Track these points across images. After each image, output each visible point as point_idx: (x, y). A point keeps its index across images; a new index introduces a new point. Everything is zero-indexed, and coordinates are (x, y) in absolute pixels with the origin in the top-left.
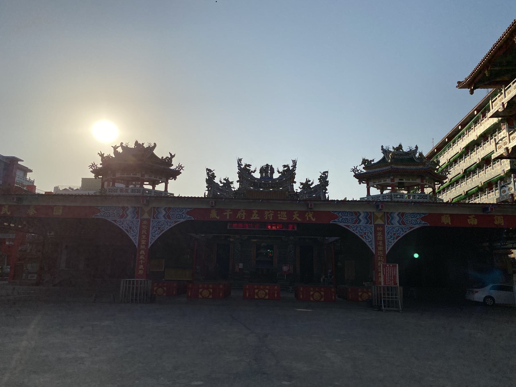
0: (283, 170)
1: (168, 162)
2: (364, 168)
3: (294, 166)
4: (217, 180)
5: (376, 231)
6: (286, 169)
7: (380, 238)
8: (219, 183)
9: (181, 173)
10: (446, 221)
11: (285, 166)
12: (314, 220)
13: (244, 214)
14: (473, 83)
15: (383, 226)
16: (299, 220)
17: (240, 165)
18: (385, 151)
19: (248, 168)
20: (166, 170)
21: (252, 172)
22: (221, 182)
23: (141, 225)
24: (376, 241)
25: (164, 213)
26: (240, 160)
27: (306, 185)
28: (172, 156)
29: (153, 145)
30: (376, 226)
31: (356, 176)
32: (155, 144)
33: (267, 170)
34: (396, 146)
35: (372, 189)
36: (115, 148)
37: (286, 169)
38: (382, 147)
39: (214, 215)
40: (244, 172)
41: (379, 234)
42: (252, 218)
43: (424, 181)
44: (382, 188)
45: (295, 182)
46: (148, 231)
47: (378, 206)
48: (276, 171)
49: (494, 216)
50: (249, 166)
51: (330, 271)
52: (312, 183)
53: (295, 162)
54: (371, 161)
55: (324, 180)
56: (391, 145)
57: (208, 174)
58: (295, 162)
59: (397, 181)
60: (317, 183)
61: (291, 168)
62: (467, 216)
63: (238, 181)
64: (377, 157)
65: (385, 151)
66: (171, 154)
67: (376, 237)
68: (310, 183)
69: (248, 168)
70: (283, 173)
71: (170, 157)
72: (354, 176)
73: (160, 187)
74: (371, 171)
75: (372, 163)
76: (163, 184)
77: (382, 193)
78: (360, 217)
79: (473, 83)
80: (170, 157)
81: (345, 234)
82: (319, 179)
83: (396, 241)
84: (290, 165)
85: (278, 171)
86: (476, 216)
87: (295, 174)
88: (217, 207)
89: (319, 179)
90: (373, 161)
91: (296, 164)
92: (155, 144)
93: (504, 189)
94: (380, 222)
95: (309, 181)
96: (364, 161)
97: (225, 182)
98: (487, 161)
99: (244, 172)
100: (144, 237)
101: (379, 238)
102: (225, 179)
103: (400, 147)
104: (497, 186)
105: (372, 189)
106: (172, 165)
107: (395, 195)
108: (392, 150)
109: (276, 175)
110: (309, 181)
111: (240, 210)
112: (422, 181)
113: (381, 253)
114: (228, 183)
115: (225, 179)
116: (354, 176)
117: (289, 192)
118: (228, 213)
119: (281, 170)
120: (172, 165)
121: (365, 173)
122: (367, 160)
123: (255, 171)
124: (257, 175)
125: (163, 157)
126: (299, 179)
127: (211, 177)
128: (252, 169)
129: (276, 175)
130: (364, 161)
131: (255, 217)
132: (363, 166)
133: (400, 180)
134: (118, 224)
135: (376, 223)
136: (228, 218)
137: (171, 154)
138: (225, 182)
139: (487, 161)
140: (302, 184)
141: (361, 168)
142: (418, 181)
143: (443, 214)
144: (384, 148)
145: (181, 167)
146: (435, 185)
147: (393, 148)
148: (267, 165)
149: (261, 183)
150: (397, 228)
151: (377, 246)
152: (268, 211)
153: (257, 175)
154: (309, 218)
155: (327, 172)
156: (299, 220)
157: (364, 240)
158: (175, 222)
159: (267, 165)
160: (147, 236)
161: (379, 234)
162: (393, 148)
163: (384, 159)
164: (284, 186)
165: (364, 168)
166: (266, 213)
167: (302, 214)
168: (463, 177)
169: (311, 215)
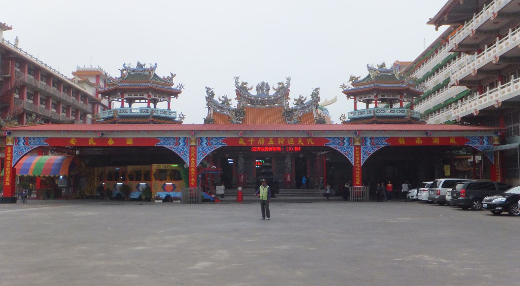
0: (278, 87)
1: (169, 81)
2: (351, 84)
3: (288, 84)
4: (216, 98)
5: (355, 151)
6: (281, 86)
7: (357, 155)
8: (218, 101)
9: (181, 92)
10: (402, 142)
11: (280, 84)
12: (313, 144)
13: (263, 141)
14: (437, 21)
15: (359, 146)
16: (303, 144)
17: (237, 83)
18: (370, 69)
19: (245, 85)
20: (166, 90)
21: (249, 89)
22: (220, 100)
23: (190, 150)
24: (355, 157)
25: (206, 141)
26: (237, 78)
27: (300, 102)
28: (173, 76)
29: (154, 65)
30: (355, 146)
31: (345, 92)
32: (156, 64)
33: (263, 87)
34: (380, 64)
35: (359, 103)
36: (122, 71)
37: (281, 86)
38: (368, 65)
39: (241, 142)
40: (242, 91)
41: (357, 152)
42: (269, 144)
43: (403, 97)
44: (368, 102)
45: (289, 99)
46: (195, 155)
47: (356, 134)
48: (271, 88)
49: (433, 137)
50: (246, 83)
51: (322, 178)
52: (305, 99)
53: (289, 79)
54: (358, 78)
55: (315, 96)
56: (376, 64)
57: (207, 92)
58: (289, 79)
59: (380, 97)
60: (309, 98)
61: (285, 85)
62: (415, 138)
63: (236, 99)
64: (363, 74)
65: (370, 69)
66: (172, 74)
67: (355, 154)
68: (303, 99)
69: (245, 85)
70: (278, 90)
71: (171, 76)
72: (343, 92)
73: (162, 105)
74: (358, 87)
75: (359, 79)
76: (166, 103)
77: (367, 107)
78: (345, 141)
79: (437, 21)
80: (171, 76)
81: (334, 153)
82: (311, 95)
83: (368, 156)
84: (285, 83)
85: (274, 88)
86: (422, 138)
87: (289, 91)
88: (244, 136)
89: (311, 95)
90: (360, 78)
91: (290, 82)
92: (156, 64)
93: (457, 110)
94: (357, 144)
95: (303, 97)
96: (352, 79)
97: (224, 99)
98: (445, 84)
99: (242, 91)
100: (193, 158)
101: (357, 155)
102: (223, 97)
103: (383, 65)
104: (451, 106)
105: (359, 103)
106: (173, 84)
107: (377, 110)
108: (377, 68)
109: (272, 92)
110: (303, 97)
111: (260, 138)
112: (401, 97)
113: (358, 165)
114: (226, 101)
115: (223, 97)
116: (343, 92)
117: (285, 110)
118: (252, 141)
119: (276, 87)
120: (173, 84)
121: (353, 89)
122: (354, 77)
123: (252, 88)
124: (254, 92)
125: (164, 77)
126: (293, 96)
127: (210, 96)
128: (249, 86)
129: (272, 92)
130: (352, 79)
131: (271, 143)
132: (351, 82)
133: (382, 96)
134: (173, 150)
135: (355, 144)
136: (252, 144)
137: (172, 74)
138: (224, 99)
139: (445, 84)
140: (296, 100)
141: (349, 86)
142: (398, 97)
143: (400, 137)
144: (370, 65)
145: (181, 86)
146: (413, 99)
147: (378, 65)
148: (263, 82)
149: (257, 101)
150: (369, 148)
151: (355, 160)
152: (281, 138)
153: (254, 92)
154: (310, 142)
155: (319, 88)
156: (303, 144)
157: (347, 157)
158: (215, 148)
159: (263, 82)
160: (195, 158)
161: (357, 152)
162: (378, 65)
163: (369, 75)
164: (279, 102)
165: (351, 84)
166: (279, 140)
167: (304, 140)
168: (434, 93)
169: (311, 141)
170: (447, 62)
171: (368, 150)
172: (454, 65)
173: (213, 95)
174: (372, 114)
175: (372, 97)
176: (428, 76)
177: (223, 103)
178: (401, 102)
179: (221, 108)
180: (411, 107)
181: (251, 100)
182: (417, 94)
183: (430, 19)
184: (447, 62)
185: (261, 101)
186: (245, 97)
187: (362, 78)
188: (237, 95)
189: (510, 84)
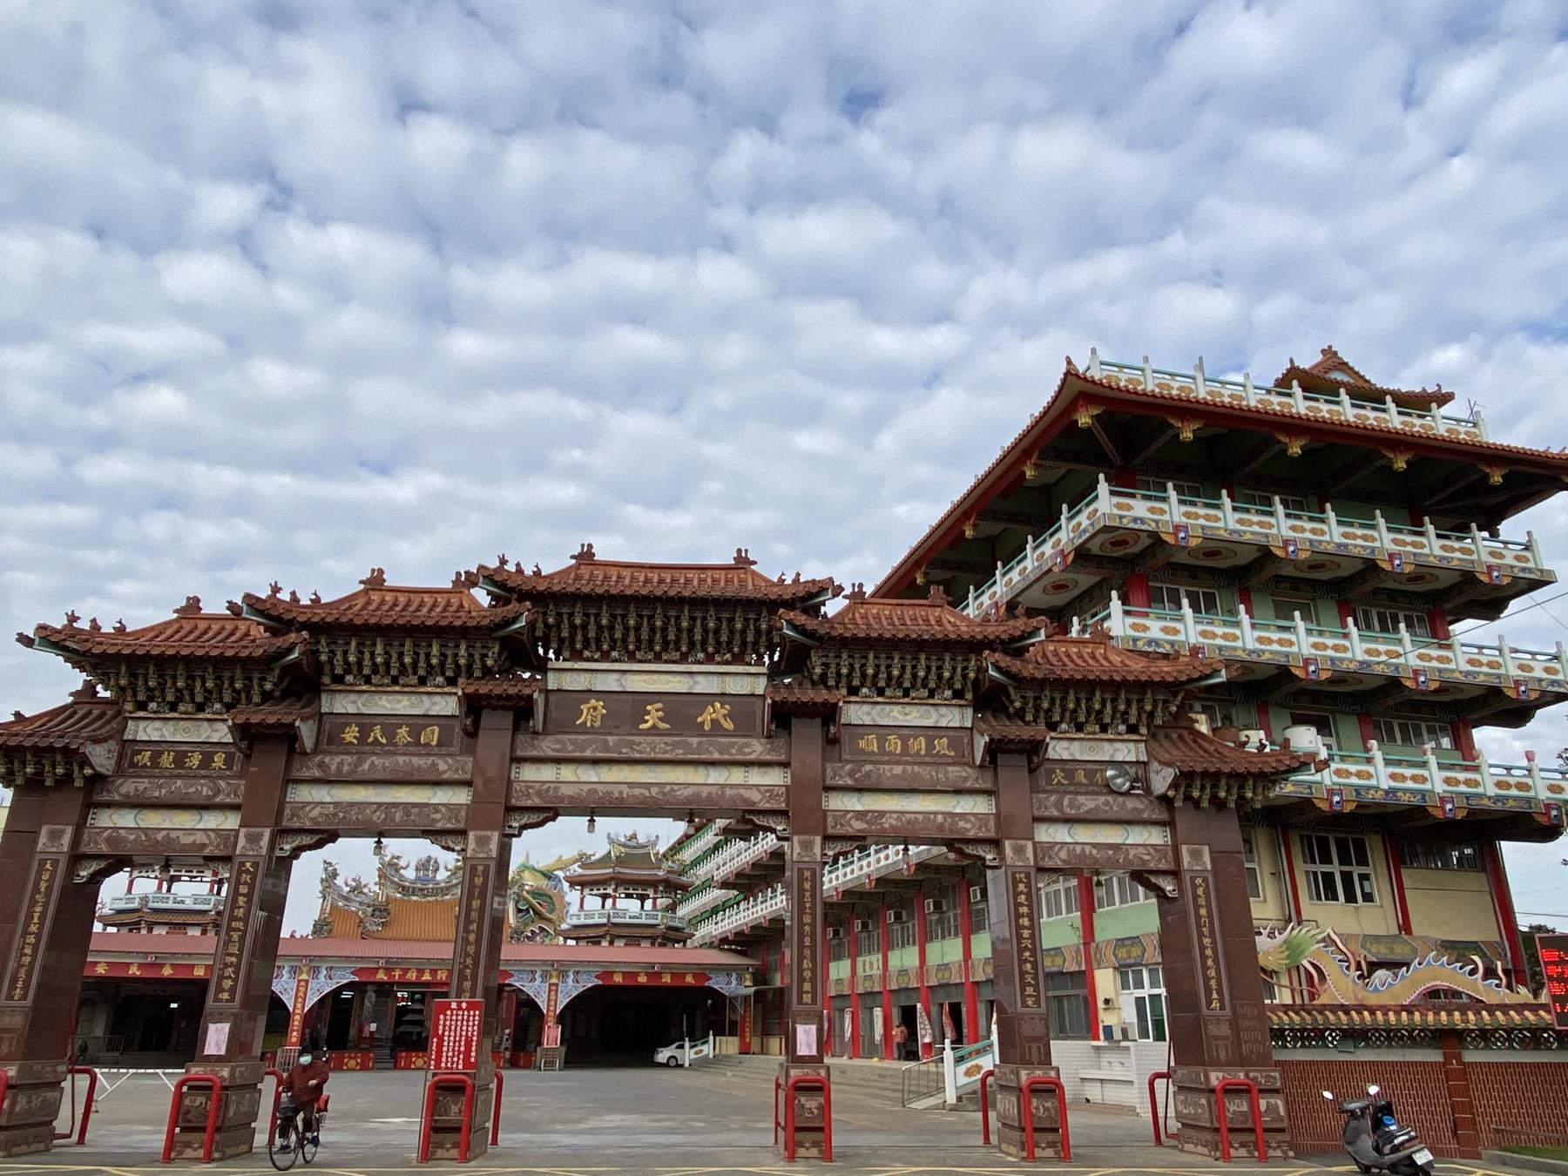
4: (339, 881)
124: (410, 874)
128: (402, 863)
153: (410, 874)
170: (716, 848)
171: (570, 989)
172: (719, 858)
173: (335, 875)
174: (604, 921)
175: (610, 891)
176: (696, 862)
177: (353, 890)
178: (655, 899)
179: (347, 899)
180: (672, 908)
181: (404, 888)
182: (684, 888)
183: (17, 714)
184: (716, 848)
185: (421, 890)
186: (393, 882)
187: (597, 856)
188: (380, 877)
189: (1060, 528)
